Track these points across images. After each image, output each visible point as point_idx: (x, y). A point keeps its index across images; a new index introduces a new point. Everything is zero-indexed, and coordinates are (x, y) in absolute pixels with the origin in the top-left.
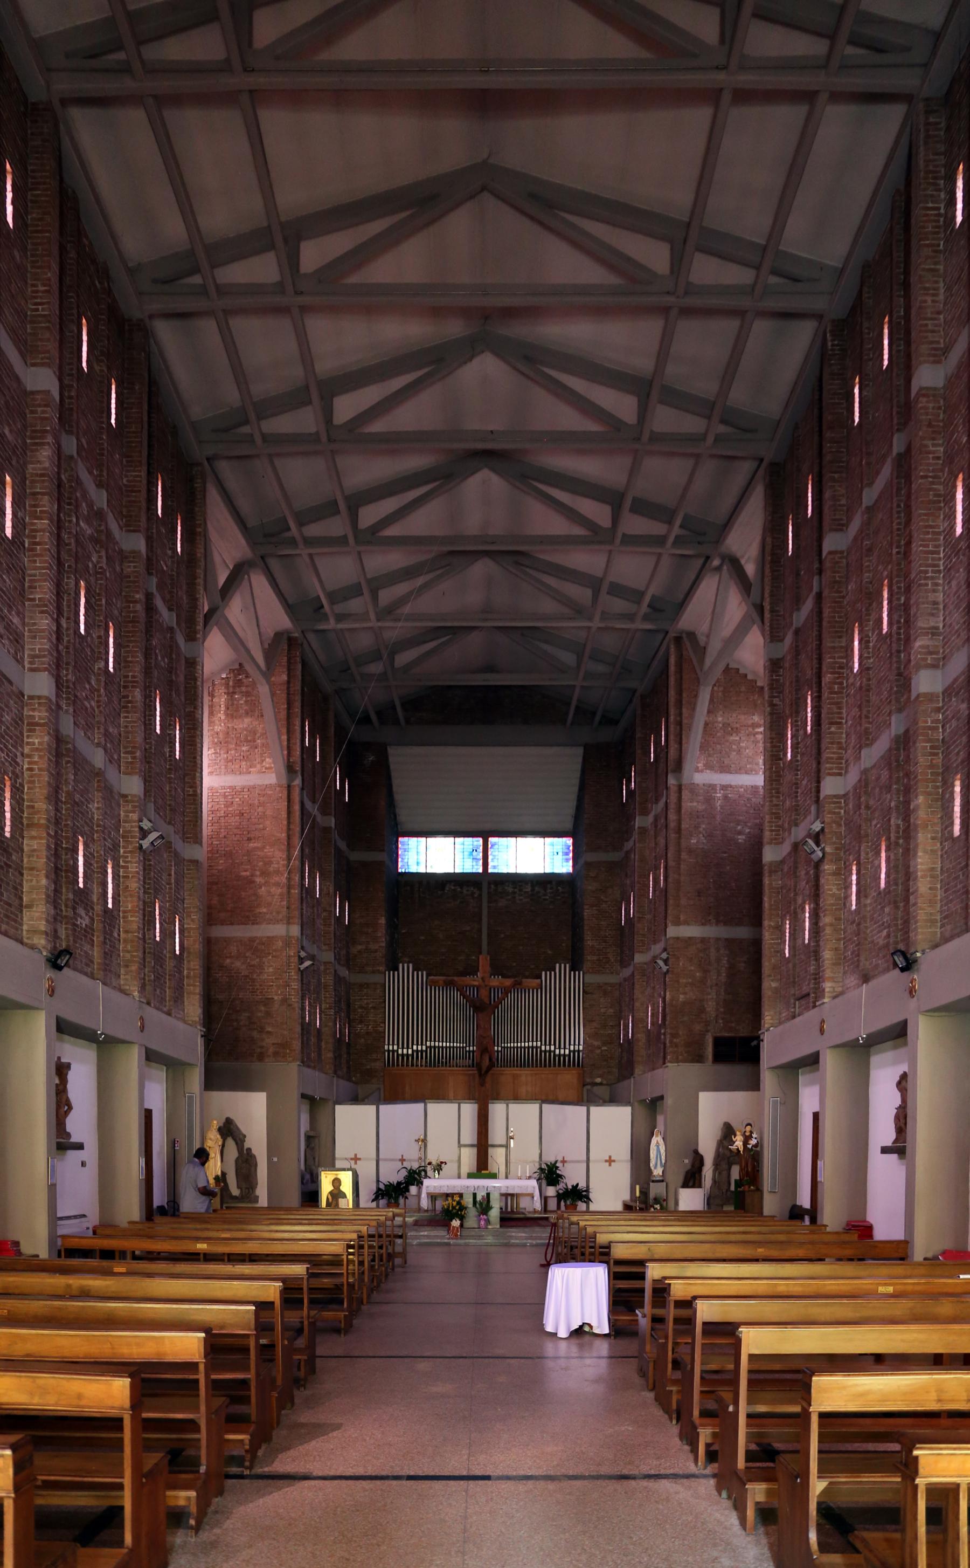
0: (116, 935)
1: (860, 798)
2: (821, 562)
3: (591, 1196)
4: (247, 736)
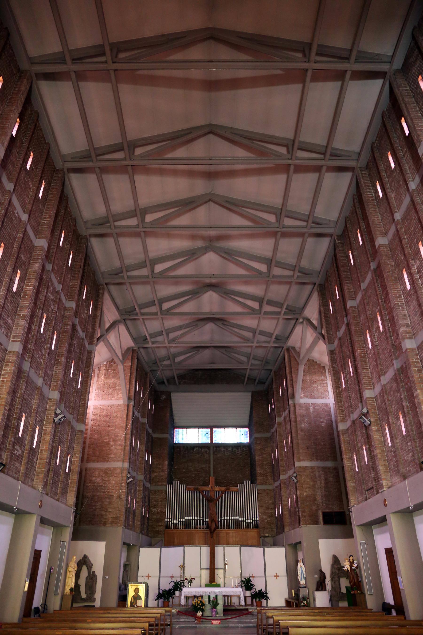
0: (35, 460)
1: (384, 396)
3: (268, 596)
4: (112, 385)
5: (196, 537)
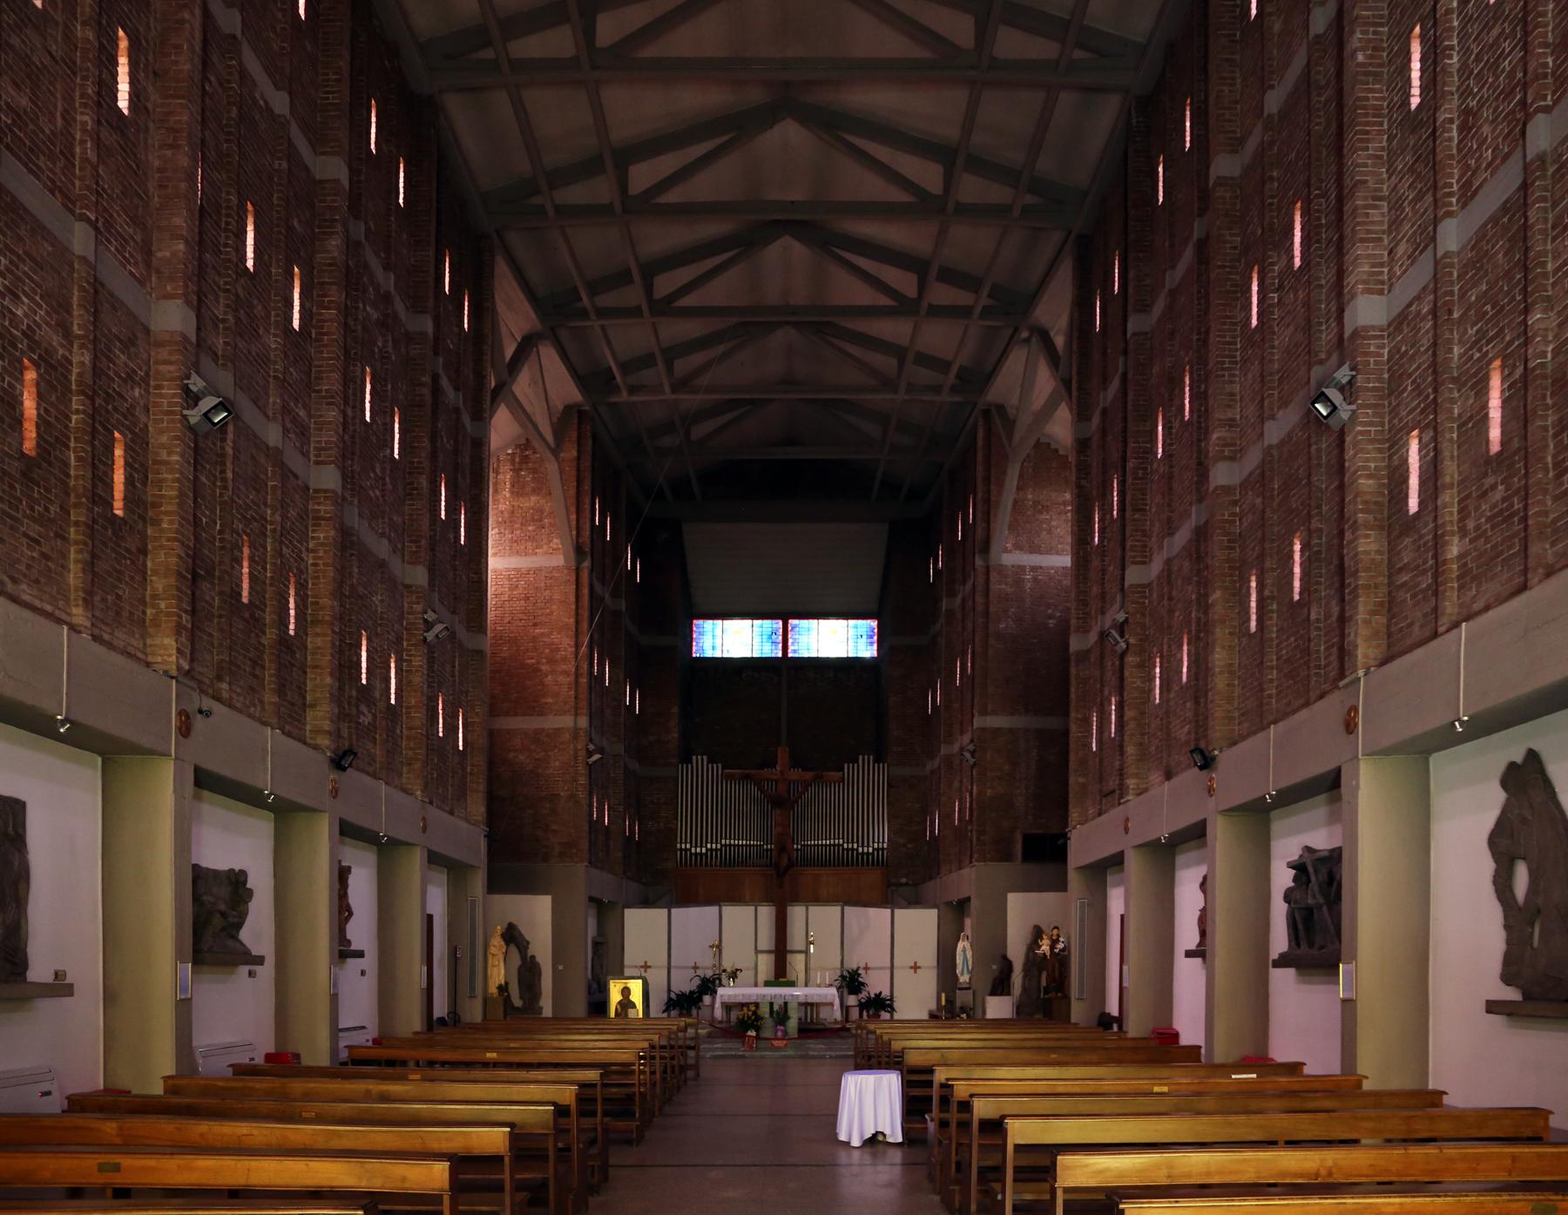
2: (1126, 341)
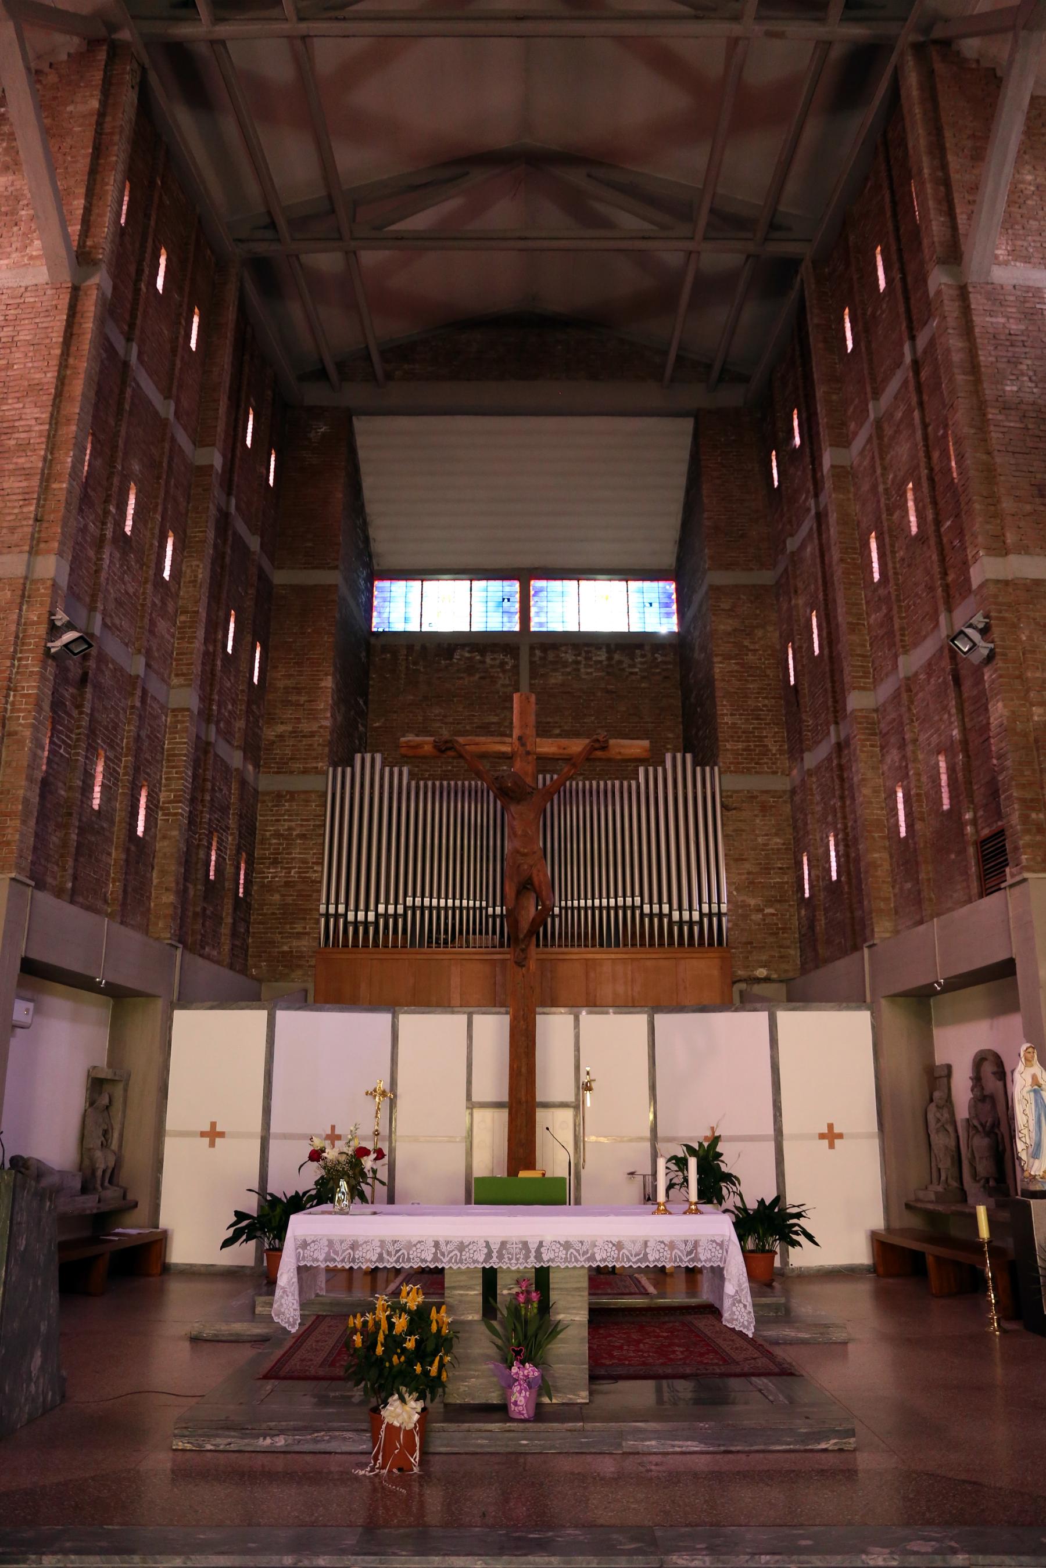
5: (455, 980)
